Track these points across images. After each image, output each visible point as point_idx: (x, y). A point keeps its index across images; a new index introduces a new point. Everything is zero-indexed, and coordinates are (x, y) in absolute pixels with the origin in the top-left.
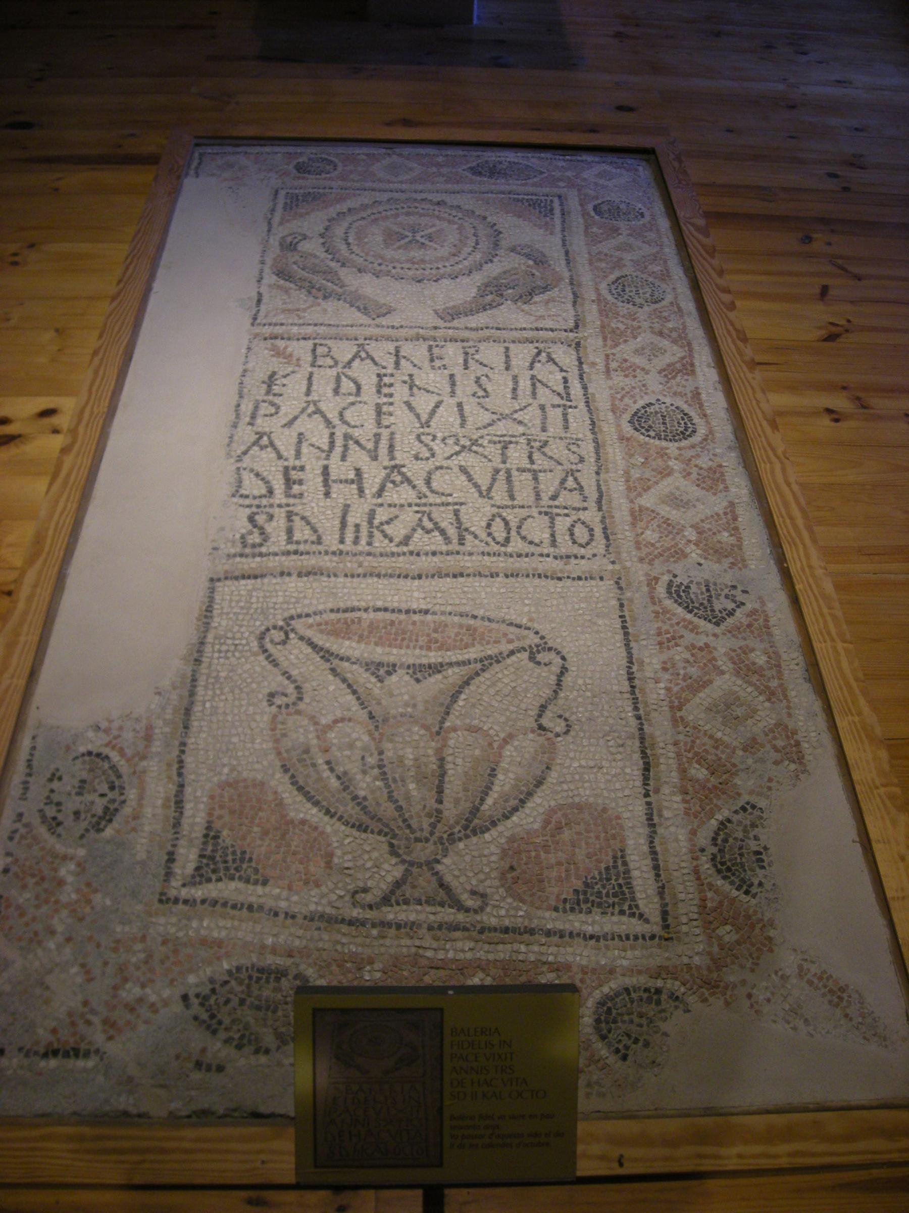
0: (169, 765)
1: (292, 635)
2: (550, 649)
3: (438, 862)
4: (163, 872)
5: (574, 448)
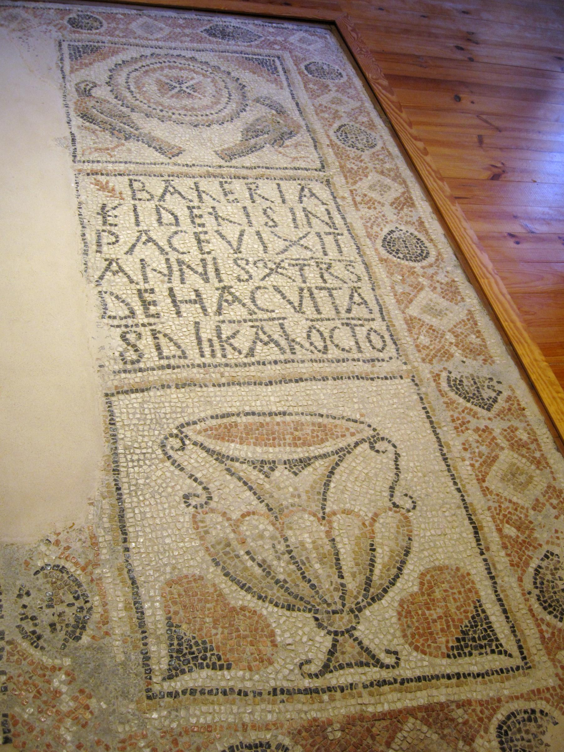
2: (383, 439)
3: (354, 628)
4: (143, 670)
5: (349, 268)
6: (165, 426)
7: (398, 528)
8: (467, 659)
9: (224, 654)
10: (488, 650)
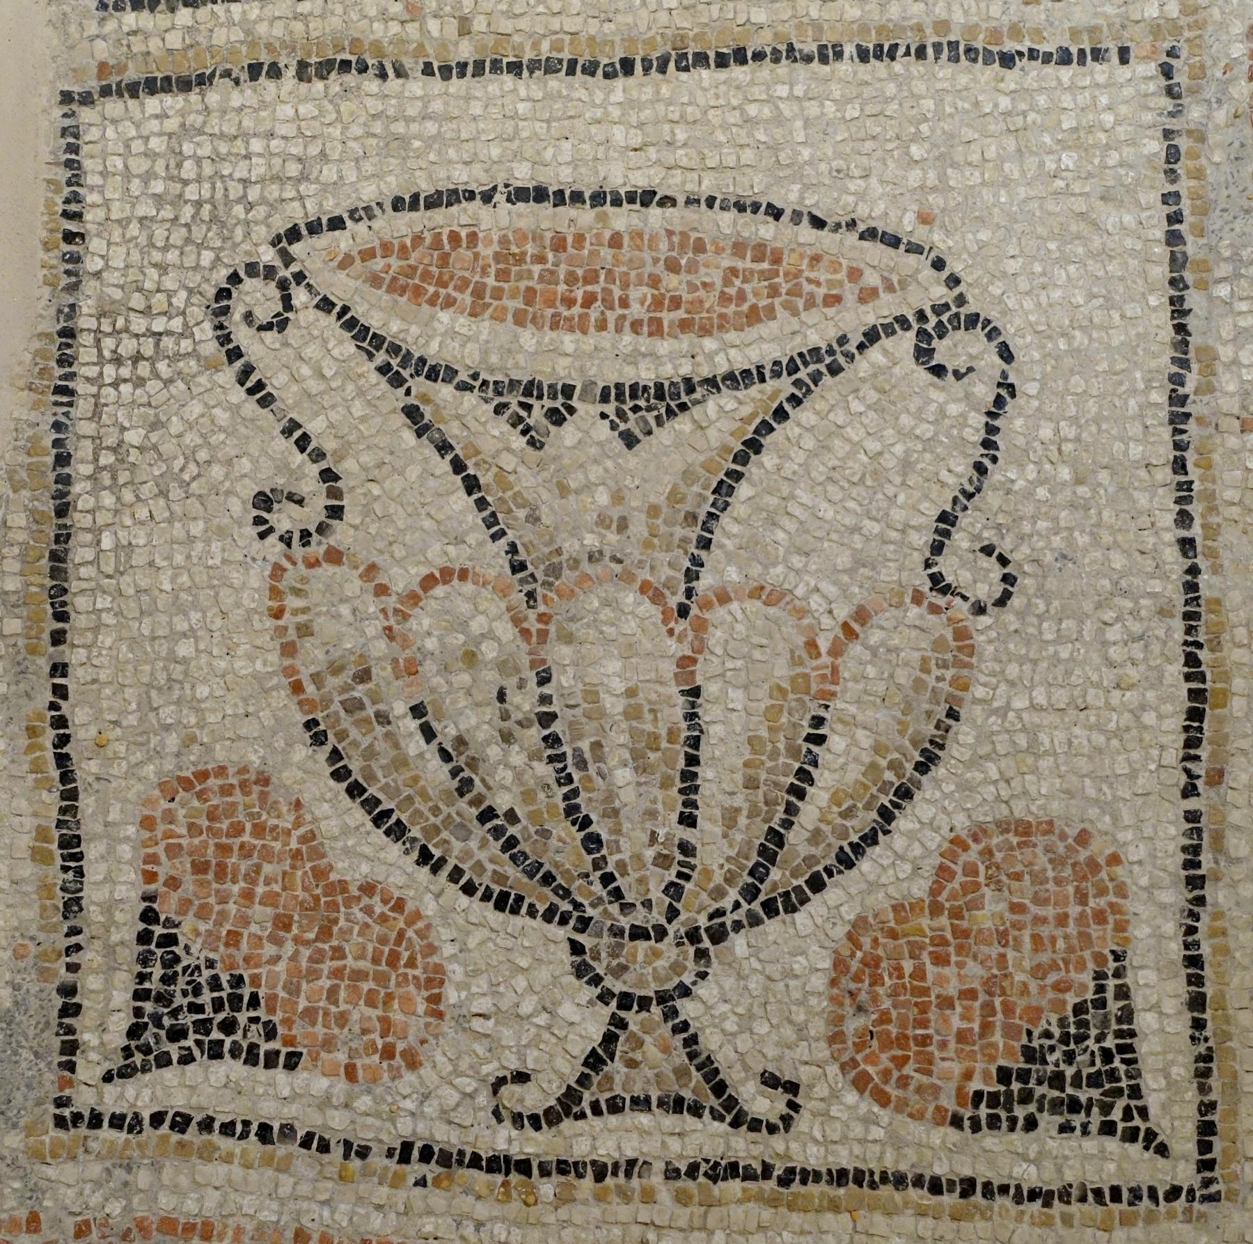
0: (32, 732)
1: (300, 296)
2: (972, 321)
3: (685, 991)
4: (56, 1043)
6: (239, 233)
7: (925, 669)
8: (1018, 1137)
9: (288, 1022)
10: (1096, 1118)
